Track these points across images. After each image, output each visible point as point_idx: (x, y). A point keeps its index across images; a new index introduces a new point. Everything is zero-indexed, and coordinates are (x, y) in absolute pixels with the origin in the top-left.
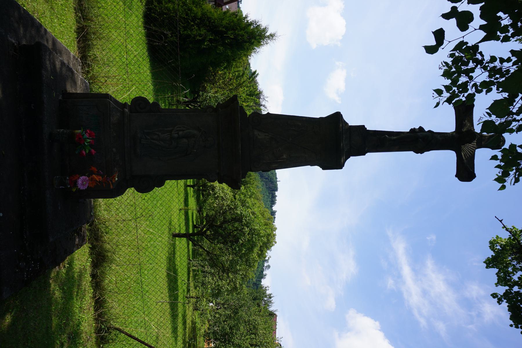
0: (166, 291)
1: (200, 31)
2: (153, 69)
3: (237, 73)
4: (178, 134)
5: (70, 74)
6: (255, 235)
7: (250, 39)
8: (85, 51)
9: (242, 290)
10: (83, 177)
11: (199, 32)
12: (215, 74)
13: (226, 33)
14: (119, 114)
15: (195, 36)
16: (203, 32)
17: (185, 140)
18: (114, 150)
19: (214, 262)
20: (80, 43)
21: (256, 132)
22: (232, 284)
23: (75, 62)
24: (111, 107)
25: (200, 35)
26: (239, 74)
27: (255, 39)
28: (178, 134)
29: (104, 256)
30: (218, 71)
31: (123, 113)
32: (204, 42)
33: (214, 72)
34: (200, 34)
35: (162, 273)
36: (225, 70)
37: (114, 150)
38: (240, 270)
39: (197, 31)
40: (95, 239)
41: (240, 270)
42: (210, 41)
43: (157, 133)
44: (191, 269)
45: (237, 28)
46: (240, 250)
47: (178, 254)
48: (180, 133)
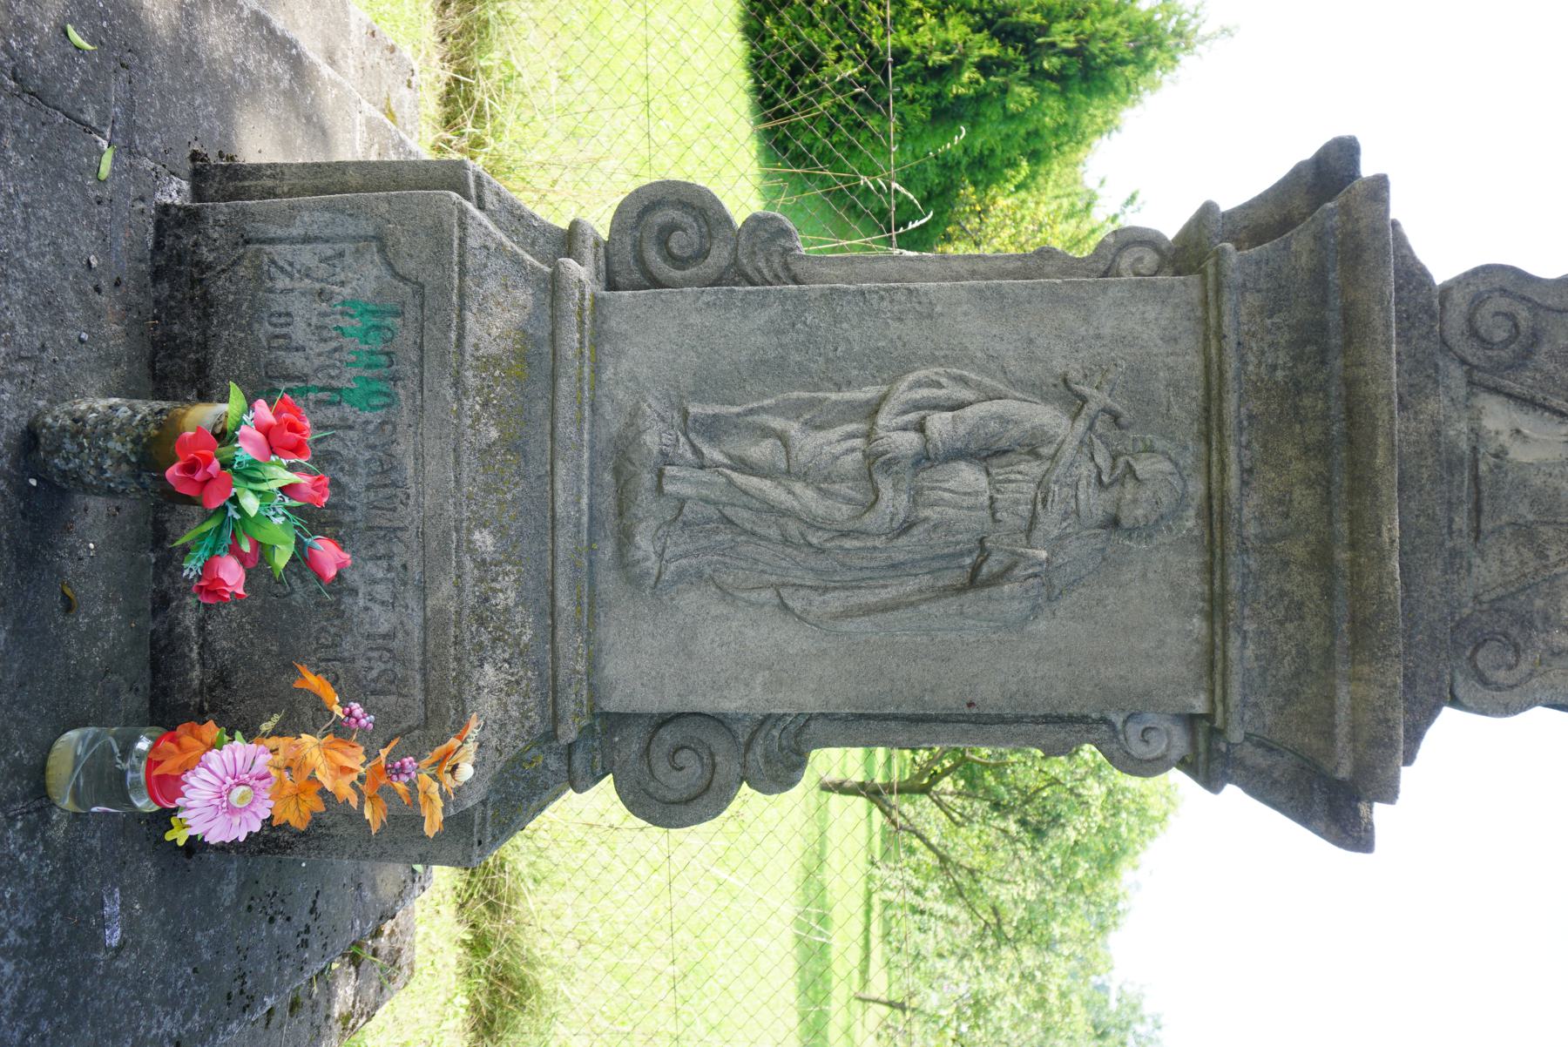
0: (791, 993)
1: (946, 30)
2: (766, 119)
3: (1065, 203)
4: (920, 428)
5: (279, 67)
6: (1129, 813)
7: (1138, 51)
8: (465, 51)
9: (1065, 1015)
10: (238, 750)
11: (941, 34)
12: (985, 211)
13: (1044, 30)
14: (524, 296)
15: (927, 50)
16: (957, 30)
17: (968, 476)
18: (484, 540)
19: (961, 883)
20: (449, 12)
21: (1497, 417)
22: (1031, 990)
23: (375, 56)
24: (472, 242)
25: (946, 48)
26: (1073, 205)
27: (1160, 46)
28: (920, 428)
29: (521, 985)
30: (994, 199)
31: (553, 286)
32: (959, 74)
33: (980, 201)
34: (946, 43)
35: (784, 902)
36: (1023, 194)
37: (484, 540)
38: (1063, 939)
39: (932, 30)
40: (489, 905)
41: (1063, 939)
42: (985, 66)
43: (777, 423)
44: (875, 899)
45: (1087, 10)
46: (1069, 867)
47: (834, 859)
48: (939, 423)
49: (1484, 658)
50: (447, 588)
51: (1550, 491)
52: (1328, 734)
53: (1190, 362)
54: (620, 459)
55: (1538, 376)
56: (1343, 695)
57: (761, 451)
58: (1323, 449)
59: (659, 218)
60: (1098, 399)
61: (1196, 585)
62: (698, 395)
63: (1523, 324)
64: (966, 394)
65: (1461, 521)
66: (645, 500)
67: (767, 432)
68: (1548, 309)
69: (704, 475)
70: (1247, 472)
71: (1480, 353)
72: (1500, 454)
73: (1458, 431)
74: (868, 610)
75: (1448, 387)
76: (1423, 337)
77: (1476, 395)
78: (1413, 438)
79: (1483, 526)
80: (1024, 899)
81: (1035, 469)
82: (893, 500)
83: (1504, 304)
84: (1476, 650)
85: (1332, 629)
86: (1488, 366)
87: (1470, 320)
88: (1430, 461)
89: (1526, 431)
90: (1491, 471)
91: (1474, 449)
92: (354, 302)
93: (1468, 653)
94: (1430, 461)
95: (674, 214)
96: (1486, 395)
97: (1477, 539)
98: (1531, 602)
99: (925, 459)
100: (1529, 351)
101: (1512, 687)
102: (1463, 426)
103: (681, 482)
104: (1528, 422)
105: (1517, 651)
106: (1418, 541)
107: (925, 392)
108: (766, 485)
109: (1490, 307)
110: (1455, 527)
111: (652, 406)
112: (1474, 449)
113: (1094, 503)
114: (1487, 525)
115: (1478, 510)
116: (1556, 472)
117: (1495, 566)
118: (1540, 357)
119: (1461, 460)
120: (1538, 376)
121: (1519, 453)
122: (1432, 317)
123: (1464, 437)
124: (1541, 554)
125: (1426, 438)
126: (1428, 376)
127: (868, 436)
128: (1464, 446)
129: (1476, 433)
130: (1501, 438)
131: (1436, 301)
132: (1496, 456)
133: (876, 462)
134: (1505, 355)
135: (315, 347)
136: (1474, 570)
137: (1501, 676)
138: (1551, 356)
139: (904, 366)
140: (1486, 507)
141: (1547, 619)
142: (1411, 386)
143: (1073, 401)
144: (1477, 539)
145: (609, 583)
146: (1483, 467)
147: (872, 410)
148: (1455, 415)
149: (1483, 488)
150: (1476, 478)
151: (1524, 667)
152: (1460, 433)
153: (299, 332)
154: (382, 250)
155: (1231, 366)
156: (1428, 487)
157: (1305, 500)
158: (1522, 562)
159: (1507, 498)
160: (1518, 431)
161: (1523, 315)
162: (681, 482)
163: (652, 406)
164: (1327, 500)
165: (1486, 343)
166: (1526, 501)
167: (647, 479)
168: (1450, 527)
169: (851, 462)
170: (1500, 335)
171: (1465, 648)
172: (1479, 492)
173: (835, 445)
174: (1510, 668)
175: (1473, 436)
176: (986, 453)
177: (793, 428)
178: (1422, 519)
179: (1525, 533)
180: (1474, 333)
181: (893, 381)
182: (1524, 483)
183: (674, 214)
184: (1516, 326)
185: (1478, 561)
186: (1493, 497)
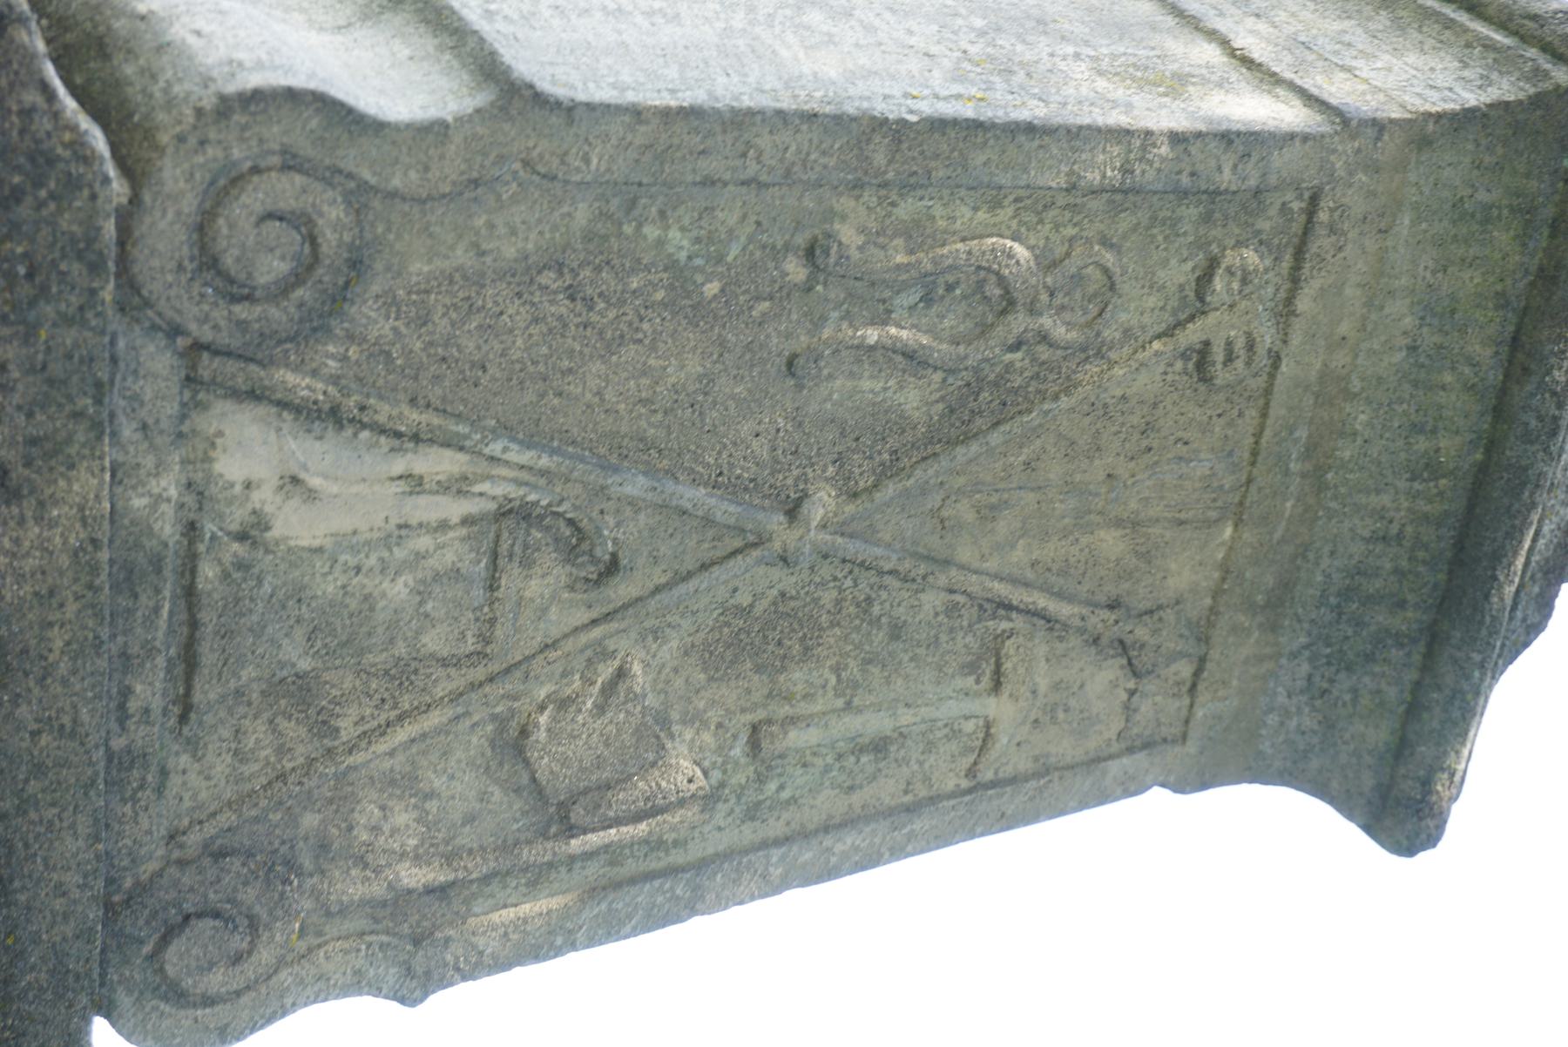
49: (175, 958)
51: (353, 604)
55: (353, 352)
63: (329, 240)
65: (149, 690)
68: (393, 195)
71: (220, 315)
72: (252, 533)
73: (157, 499)
75: (136, 398)
76: (67, 320)
77: (202, 406)
78: (30, 564)
79: (197, 697)
83: (286, 190)
84: (165, 941)
86: (235, 343)
87: (202, 228)
88: (71, 608)
89: (315, 482)
90: (226, 575)
91: (191, 529)
93: (147, 949)
94: (71, 608)
96: (228, 405)
97: (183, 718)
98: (292, 819)
100: (338, 299)
101: (238, 994)
102: (169, 485)
104: (319, 456)
105: (253, 925)
106: (34, 786)
109: (253, 199)
110: (133, 705)
112: (191, 529)
114: (206, 692)
115: (189, 660)
116: (373, 561)
117: (221, 766)
118: (369, 315)
119: (157, 563)
120: (353, 352)
121: (296, 526)
122: (96, 268)
123: (167, 509)
124: (324, 727)
125: (64, 561)
126: (77, 415)
128: (167, 528)
129: (198, 491)
130: (256, 497)
131: (109, 228)
132: (242, 537)
134: (278, 315)
136: (175, 781)
137: (216, 981)
138: (390, 303)
140: (208, 655)
141: (323, 847)
142: (33, 441)
144: (183, 718)
146: (208, 572)
148: (149, 462)
149: (205, 616)
150: (189, 593)
151: (265, 955)
152: (158, 499)
156: (64, 668)
158: (281, 751)
159: (258, 631)
160: (295, 480)
161: (332, 213)
165: (237, 291)
166: (299, 633)
168: (122, 707)
170: (271, 269)
171: (142, 942)
172: (194, 624)
174: (237, 959)
175: (190, 499)
178: (45, 739)
180: (207, 261)
182: (299, 594)
184: (312, 240)
185: (185, 759)
186: (226, 634)
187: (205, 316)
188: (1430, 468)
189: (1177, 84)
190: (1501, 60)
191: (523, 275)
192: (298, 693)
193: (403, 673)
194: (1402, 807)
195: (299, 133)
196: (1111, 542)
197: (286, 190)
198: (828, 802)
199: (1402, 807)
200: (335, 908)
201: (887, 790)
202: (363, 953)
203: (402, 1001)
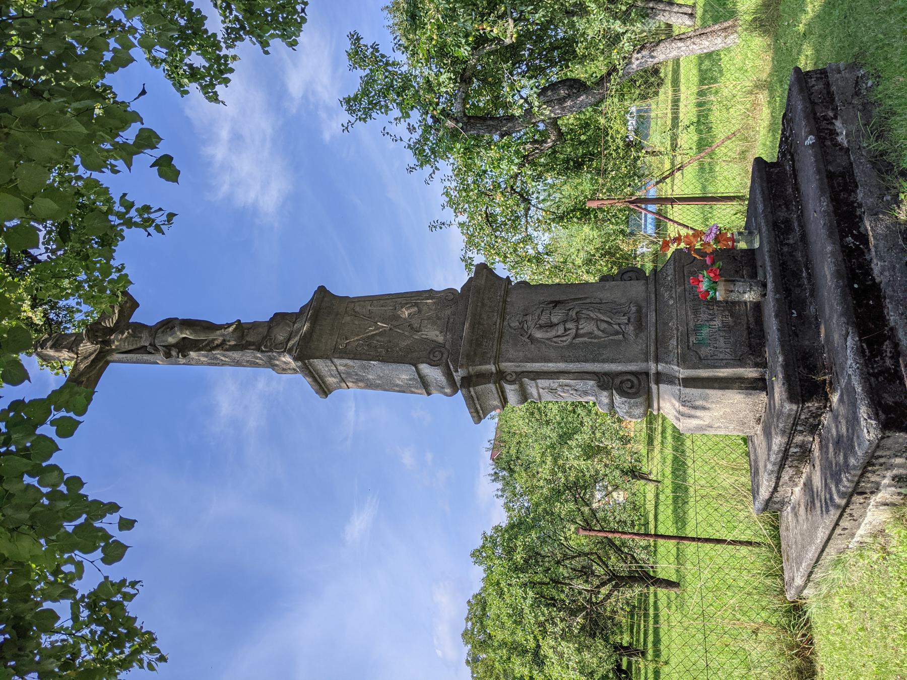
17: (555, 320)
21: (440, 339)
50: (679, 290)
52: (487, 276)
53: (503, 347)
54: (640, 326)
56: (483, 282)
57: (603, 326)
58: (479, 323)
59: (633, 390)
60: (525, 339)
61: (508, 306)
62: (620, 341)
64: (555, 339)
65: (452, 320)
66: (633, 317)
67: (602, 331)
69: (619, 321)
70: (495, 324)
72: (441, 332)
74: (580, 299)
80: (561, 503)
81: (540, 322)
82: (573, 314)
85: (483, 293)
92: (707, 346)
95: (630, 391)
99: (565, 322)
103: (624, 320)
104: (435, 338)
107: (564, 339)
108: (603, 318)
111: (632, 337)
113: (529, 318)
121: (438, 333)
127: (578, 329)
129: (445, 336)
133: (577, 321)
135: (717, 337)
139: (568, 346)
143: (530, 337)
145: (644, 304)
147: (577, 336)
153: (722, 340)
154: (700, 357)
155: (495, 343)
157: (484, 316)
162: (624, 320)
163: (632, 337)
164: (481, 315)
167: (632, 320)
169: (582, 322)
173: (587, 327)
176: (552, 326)
177: (596, 332)
179: (439, 318)
181: (571, 343)
183: (630, 391)
187: (443, 350)
188: (321, 325)
189: (345, 365)
190: (311, 365)
191: (415, 351)
192: (439, 318)
193: (429, 319)
194: (322, 290)
195: (433, 363)
196: (356, 323)
197: (435, 359)
198: (389, 301)
199: (322, 290)
200: (568, 495)
201: (382, 302)
202: (447, 6)
203: (299, 26)
